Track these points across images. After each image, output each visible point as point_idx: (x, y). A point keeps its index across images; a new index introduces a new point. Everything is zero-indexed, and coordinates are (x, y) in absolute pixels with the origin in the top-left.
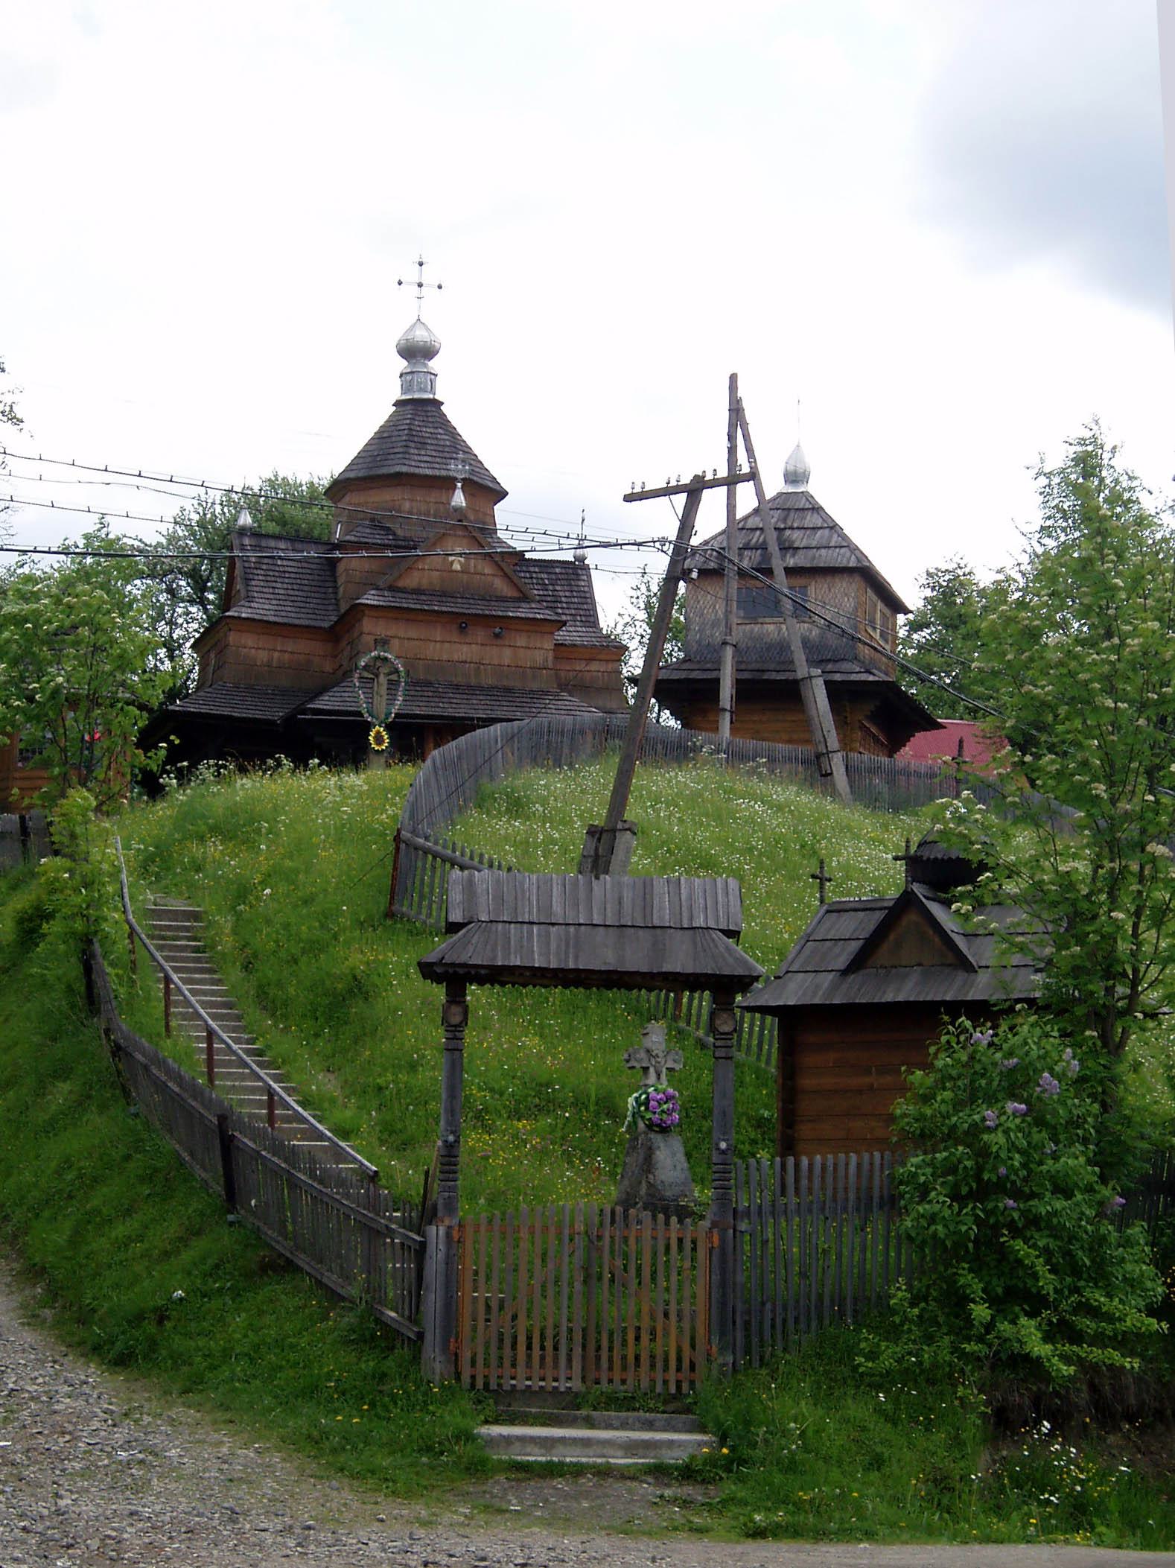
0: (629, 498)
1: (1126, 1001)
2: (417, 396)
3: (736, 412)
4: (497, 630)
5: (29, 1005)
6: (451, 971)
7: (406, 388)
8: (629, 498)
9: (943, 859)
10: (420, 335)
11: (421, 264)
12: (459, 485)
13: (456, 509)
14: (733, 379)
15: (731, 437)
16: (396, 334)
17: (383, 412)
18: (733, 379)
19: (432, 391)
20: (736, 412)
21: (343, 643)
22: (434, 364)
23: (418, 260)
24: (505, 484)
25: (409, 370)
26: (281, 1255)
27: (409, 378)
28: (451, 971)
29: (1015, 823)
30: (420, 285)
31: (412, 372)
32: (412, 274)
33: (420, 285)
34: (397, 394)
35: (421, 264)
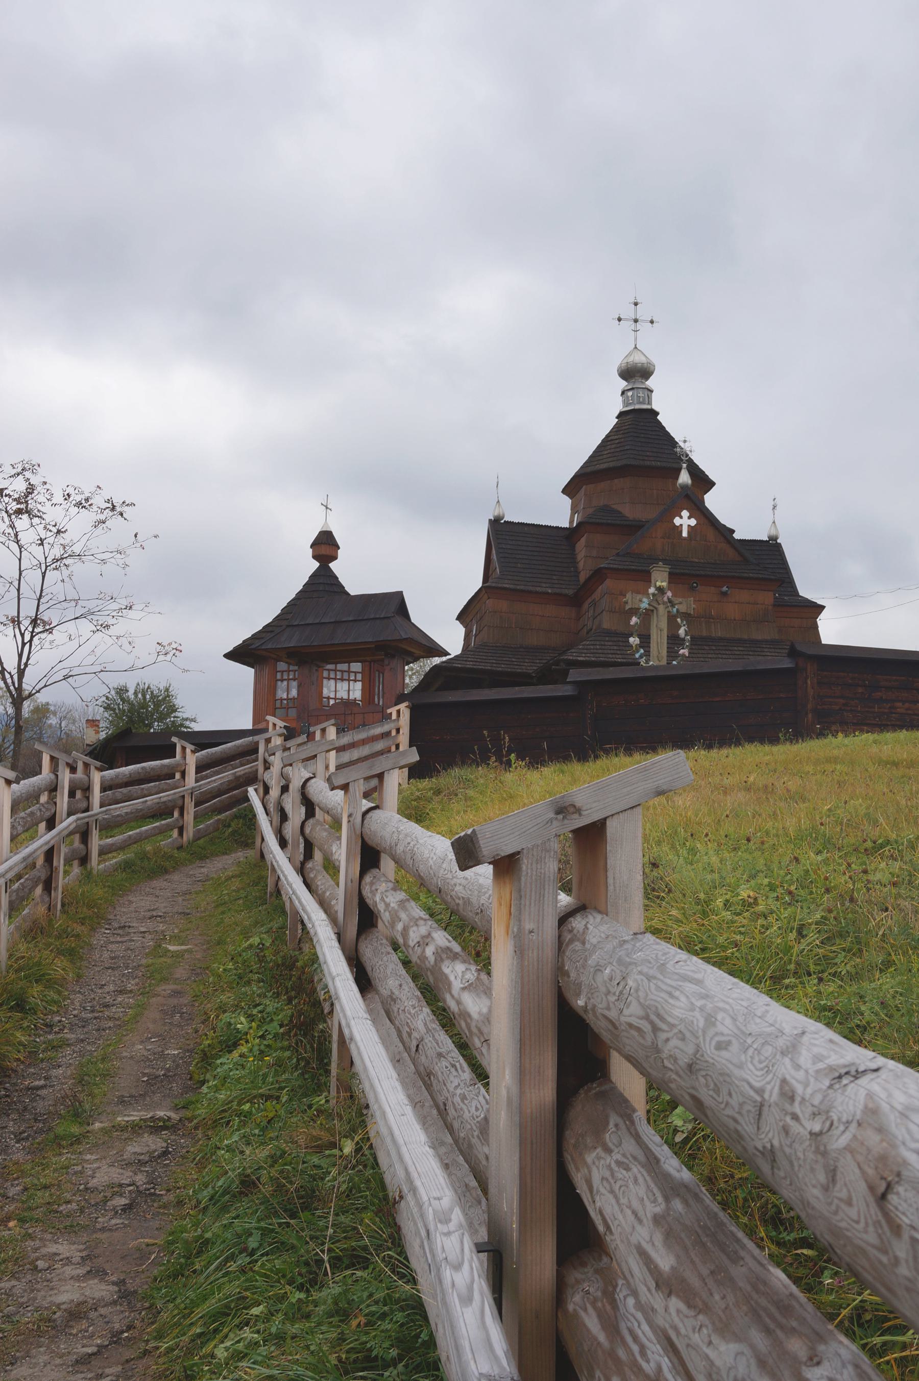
2: (638, 407)
4: (725, 589)
5: (14, 1282)
7: (626, 403)
10: (638, 359)
11: (636, 304)
12: (684, 465)
13: (684, 487)
15: (26, 665)
16: (618, 358)
19: (650, 403)
21: (586, 606)
22: (650, 383)
23: (633, 300)
24: (712, 477)
25: (630, 387)
27: (630, 394)
30: (636, 321)
33: (636, 321)
34: (618, 406)
35: (636, 304)
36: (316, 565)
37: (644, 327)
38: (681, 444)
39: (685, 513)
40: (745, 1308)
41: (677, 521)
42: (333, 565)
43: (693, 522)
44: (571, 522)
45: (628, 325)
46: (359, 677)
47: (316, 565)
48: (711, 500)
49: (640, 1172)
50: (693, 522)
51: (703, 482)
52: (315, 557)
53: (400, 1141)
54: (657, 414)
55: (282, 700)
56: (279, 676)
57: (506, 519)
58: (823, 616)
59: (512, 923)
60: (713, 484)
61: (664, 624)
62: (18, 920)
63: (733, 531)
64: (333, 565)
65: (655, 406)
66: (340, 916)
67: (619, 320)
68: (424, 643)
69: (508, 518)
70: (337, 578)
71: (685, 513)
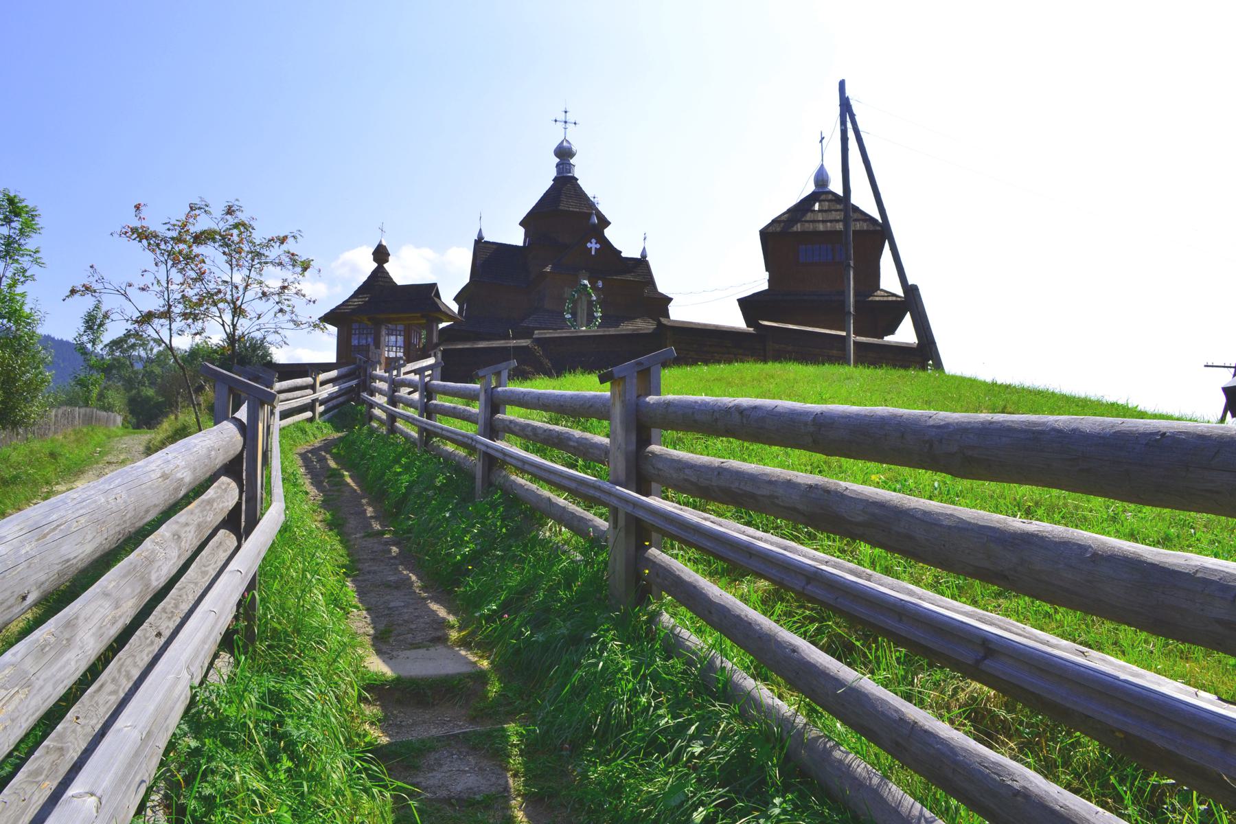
0: (1206, 366)
1: (839, 191)
3: (846, 107)
6: (474, 443)
8: (1206, 366)
9: (1102, 555)
11: (566, 112)
14: (842, 84)
15: (843, 123)
17: (548, 183)
18: (842, 84)
20: (846, 107)
26: (664, 552)
28: (474, 443)
29: (153, 398)
30: (566, 122)
31: (563, 164)
32: (561, 117)
33: (566, 122)
35: (566, 112)
37: (570, 127)
38: (592, 199)
39: (594, 241)
41: (589, 245)
42: (386, 266)
43: (598, 246)
44: (525, 242)
45: (561, 125)
46: (402, 333)
48: (608, 233)
50: (598, 246)
51: (605, 223)
52: (375, 260)
55: (400, 335)
56: (353, 332)
57: (485, 239)
58: (671, 304)
60: (738, 300)
61: (585, 307)
63: (621, 252)
64: (386, 266)
66: (798, 227)
67: (556, 121)
68: (450, 314)
69: (487, 238)
70: (388, 273)
71: (594, 241)
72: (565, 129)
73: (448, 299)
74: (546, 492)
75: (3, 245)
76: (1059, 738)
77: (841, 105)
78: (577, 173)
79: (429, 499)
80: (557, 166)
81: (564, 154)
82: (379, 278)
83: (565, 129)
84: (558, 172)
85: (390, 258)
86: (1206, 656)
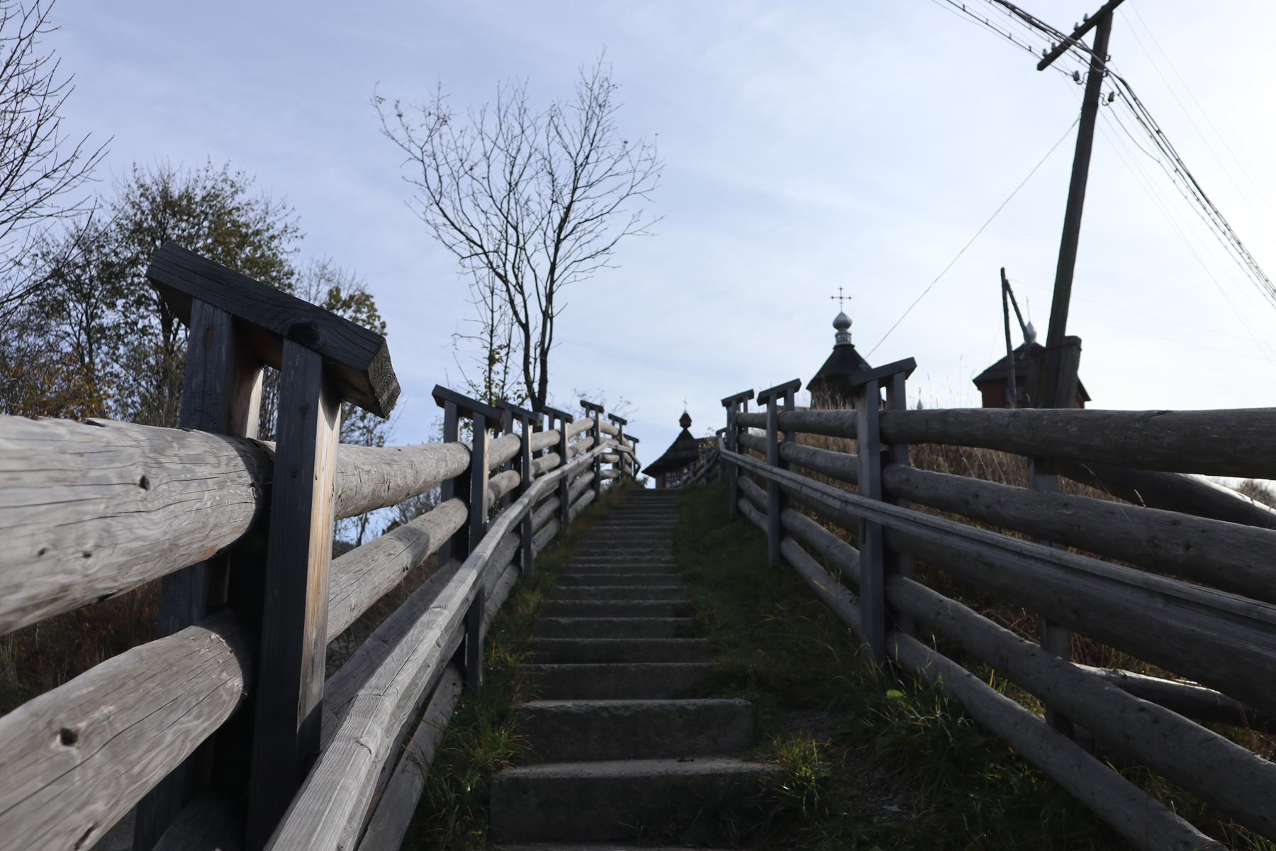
3: (1006, 286)
11: (841, 289)
14: (1003, 271)
18: (1003, 271)
20: (1006, 286)
23: (839, 287)
30: (841, 298)
32: (837, 294)
33: (841, 298)
35: (841, 289)
36: (681, 429)
37: (845, 301)
40: (825, 558)
42: (690, 429)
47: (681, 429)
49: (634, 554)
52: (682, 425)
53: (1122, 580)
54: (853, 346)
59: (29, 522)
62: (935, 648)
63: (1088, 399)
64: (690, 429)
65: (853, 343)
72: (841, 303)
73: (1088, 406)
74: (657, 497)
75: (496, 436)
76: (123, 285)
77: (1003, 286)
78: (854, 341)
79: (165, 220)
80: (836, 336)
81: (842, 325)
82: (685, 436)
83: (841, 303)
84: (837, 341)
85: (692, 423)
86: (440, 430)
